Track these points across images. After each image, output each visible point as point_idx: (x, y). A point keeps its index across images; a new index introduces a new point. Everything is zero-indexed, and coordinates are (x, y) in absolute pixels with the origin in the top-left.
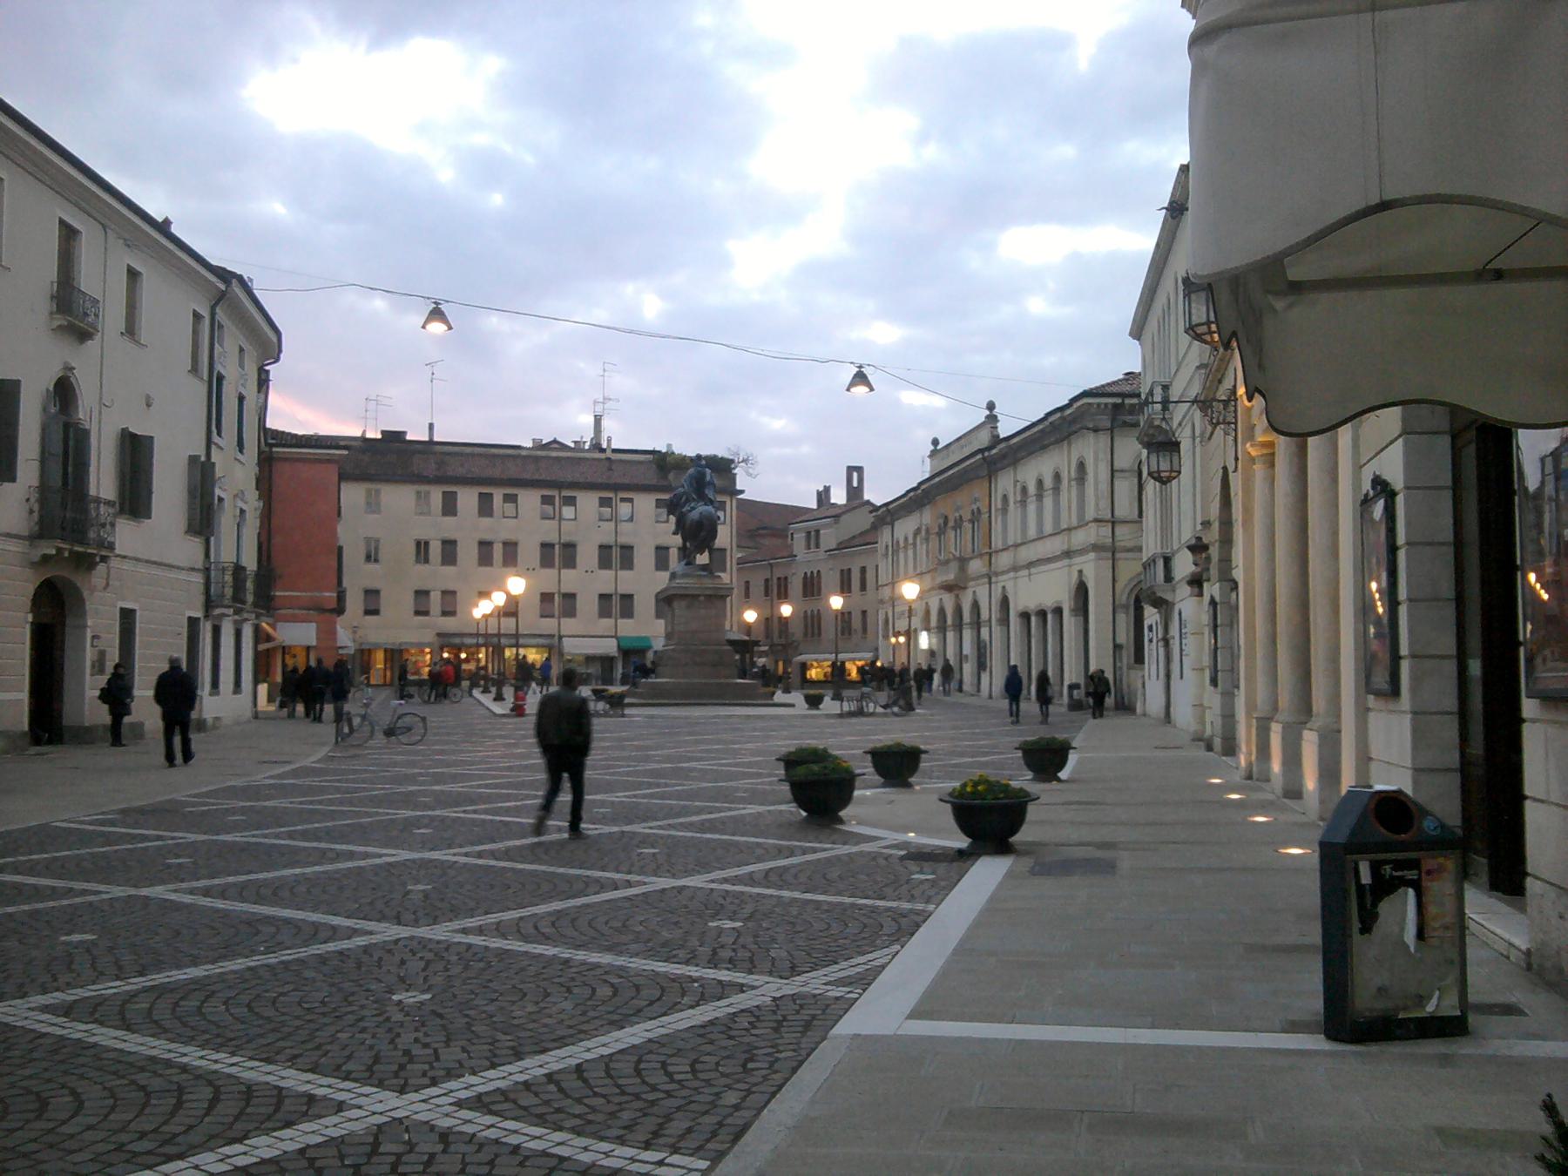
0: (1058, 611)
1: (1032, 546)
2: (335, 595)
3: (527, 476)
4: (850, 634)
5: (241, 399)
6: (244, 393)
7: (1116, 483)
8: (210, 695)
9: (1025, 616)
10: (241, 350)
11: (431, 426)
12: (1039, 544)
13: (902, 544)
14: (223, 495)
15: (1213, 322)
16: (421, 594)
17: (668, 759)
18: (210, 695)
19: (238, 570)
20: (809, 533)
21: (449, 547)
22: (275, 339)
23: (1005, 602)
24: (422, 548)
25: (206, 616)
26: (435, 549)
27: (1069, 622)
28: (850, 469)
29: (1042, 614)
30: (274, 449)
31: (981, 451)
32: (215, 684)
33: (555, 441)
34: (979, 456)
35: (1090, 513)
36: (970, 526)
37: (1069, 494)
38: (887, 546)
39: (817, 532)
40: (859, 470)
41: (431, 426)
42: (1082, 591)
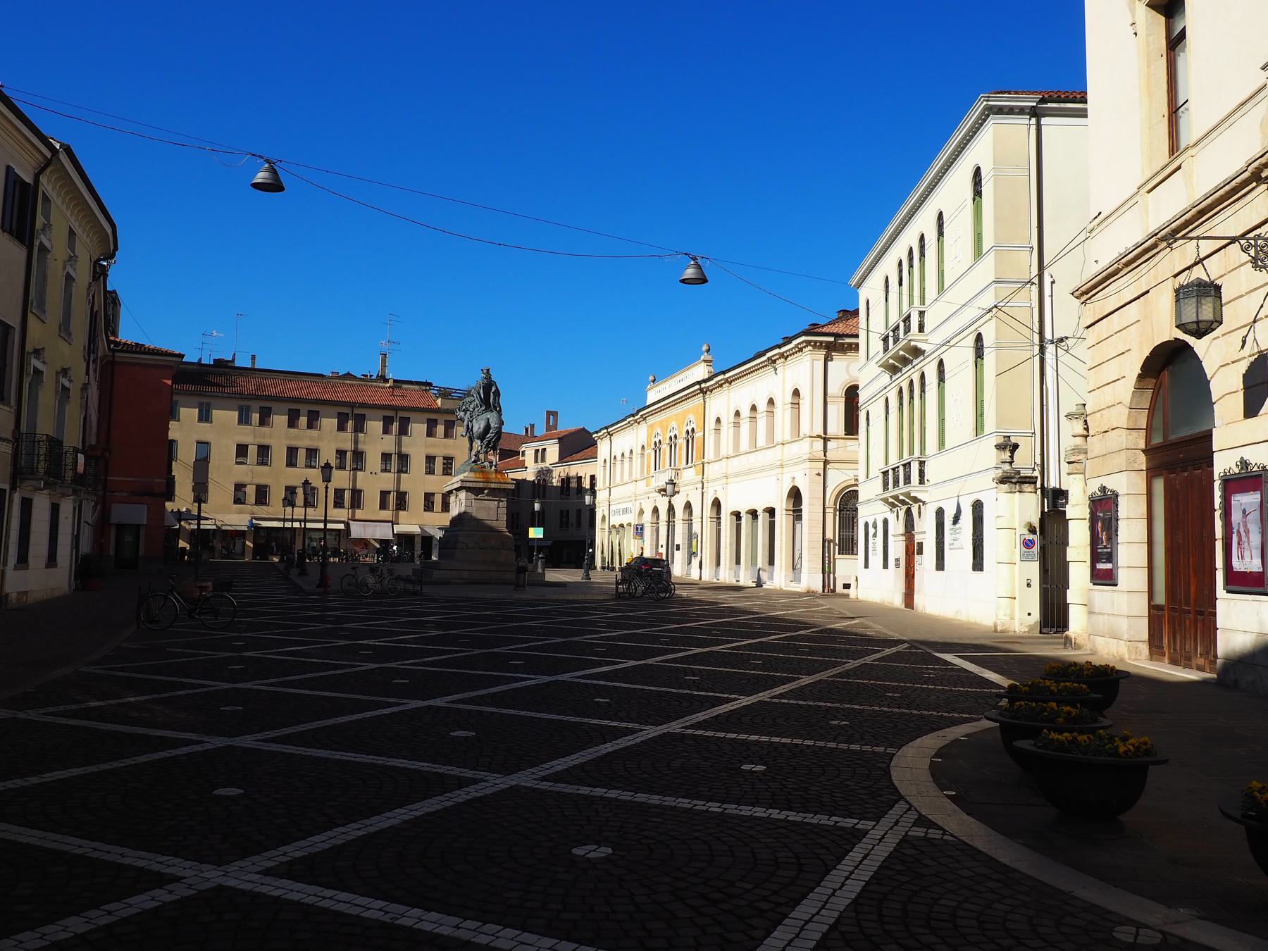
0: (771, 512)
1: (743, 458)
2: (165, 481)
3: (327, 397)
4: (567, 527)
5: (69, 279)
6: (72, 273)
7: (829, 407)
8: (16, 568)
9: (737, 515)
10: (72, 233)
11: (253, 357)
12: (735, 461)
13: (619, 457)
14: (40, 366)
15: (325, 525)
16: (239, 487)
17: (439, 625)
18: (16, 568)
19: (55, 444)
20: (538, 450)
21: (264, 451)
22: (109, 231)
23: (717, 504)
24: (242, 450)
25: (13, 488)
26: (252, 451)
27: (782, 520)
28: (549, 413)
29: (754, 514)
30: (117, 354)
31: (699, 383)
32: (23, 559)
33: (348, 374)
34: (697, 387)
35: (805, 429)
36: (669, 448)
37: (783, 412)
38: (605, 461)
39: (544, 450)
40: (555, 414)
41: (253, 357)
42: (795, 495)
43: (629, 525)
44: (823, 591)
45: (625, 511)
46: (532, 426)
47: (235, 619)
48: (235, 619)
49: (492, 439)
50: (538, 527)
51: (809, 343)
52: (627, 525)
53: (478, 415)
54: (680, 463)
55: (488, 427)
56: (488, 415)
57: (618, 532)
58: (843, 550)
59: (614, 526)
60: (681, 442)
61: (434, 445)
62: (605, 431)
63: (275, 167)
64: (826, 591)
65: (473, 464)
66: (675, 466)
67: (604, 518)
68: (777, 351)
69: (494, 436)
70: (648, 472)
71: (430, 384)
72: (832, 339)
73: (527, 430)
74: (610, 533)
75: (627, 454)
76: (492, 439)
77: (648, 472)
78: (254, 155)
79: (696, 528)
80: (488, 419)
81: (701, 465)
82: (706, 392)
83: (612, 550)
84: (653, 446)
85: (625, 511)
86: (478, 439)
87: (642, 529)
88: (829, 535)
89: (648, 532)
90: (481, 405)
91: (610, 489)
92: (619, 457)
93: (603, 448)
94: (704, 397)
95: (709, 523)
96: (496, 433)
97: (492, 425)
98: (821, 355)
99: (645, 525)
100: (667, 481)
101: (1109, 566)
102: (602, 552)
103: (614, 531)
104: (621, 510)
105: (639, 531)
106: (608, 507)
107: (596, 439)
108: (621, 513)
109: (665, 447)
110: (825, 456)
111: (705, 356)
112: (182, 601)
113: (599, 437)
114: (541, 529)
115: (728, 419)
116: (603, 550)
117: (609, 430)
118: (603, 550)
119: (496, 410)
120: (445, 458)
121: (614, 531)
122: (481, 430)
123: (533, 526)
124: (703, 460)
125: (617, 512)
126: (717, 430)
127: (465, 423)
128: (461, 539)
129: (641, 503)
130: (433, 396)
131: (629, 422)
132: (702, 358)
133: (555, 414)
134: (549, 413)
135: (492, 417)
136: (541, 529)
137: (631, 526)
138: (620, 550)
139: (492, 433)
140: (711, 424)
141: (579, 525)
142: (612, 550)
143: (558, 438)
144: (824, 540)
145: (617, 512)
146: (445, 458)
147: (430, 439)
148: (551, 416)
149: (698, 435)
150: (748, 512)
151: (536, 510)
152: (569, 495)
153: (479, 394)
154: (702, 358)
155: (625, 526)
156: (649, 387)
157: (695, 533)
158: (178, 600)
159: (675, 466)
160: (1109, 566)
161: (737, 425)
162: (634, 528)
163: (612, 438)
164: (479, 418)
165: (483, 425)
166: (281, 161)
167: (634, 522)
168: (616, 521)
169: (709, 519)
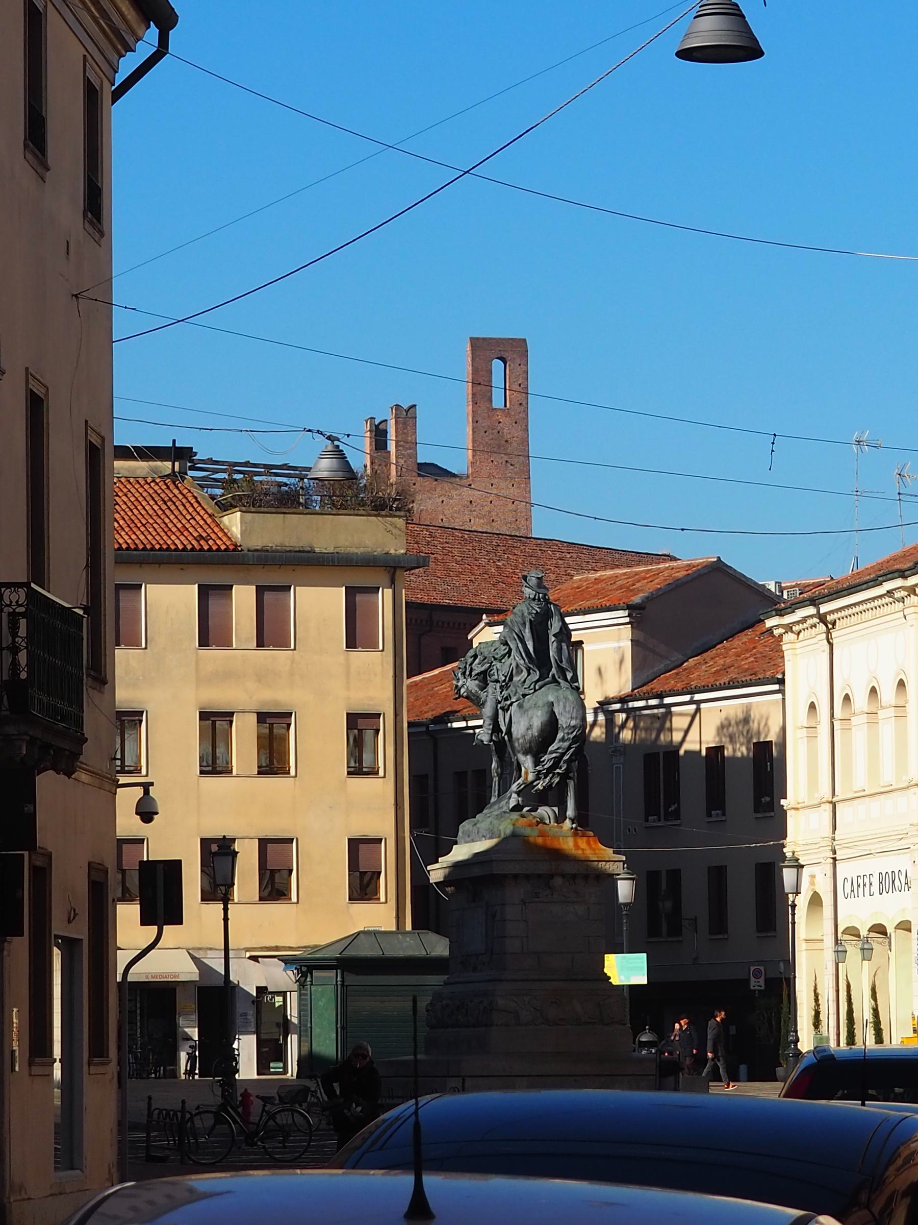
13: (860, 700)
47: (312, 1143)
48: (312, 1143)
49: (563, 754)
53: (524, 696)
55: (551, 727)
56: (549, 694)
57: (866, 953)
59: (853, 932)
61: (226, 675)
62: (811, 610)
65: (515, 815)
67: (816, 901)
69: (569, 748)
71: (182, 454)
73: (379, 435)
74: (840, 954)
75: (888, 694)
76: (563, 754)
78: (310, 431)
83: (850, 1012)
86: (525, 753)
92: (860, 700)
96: (575, 740)
97: (563, 721)
101: (757, 992)
102: (817, 1023)
103: (853, 951)
104: (875, 881)
106: (829, 869)
112: (239, 1120)
113: (789, 628)
116: (817, 1014)
117: (824, 608)
118: (817, 1014)
119: (566, 679)
120: (262, 717)
121: (853, 951)
122: (535, 732)
123: (617, 949)
125: (860, 885)
127: (488, 710)
128: (501, 1002)
130: (210, 507)
131: (890, 593)
137: (909, 930)
138: (876, 1011)
139: (563, 740)
142: (850, 1012)
145: (860, 885)
146: (262, 717)
147: (213, 654)
148: (497, 365)
151: (622, 899)
152: (677, 815)
155: (890, 930)
158: (235, 1122)
160: (757, 992)
164: (528, 702)
165: (538, 719)
166: (348, 436)
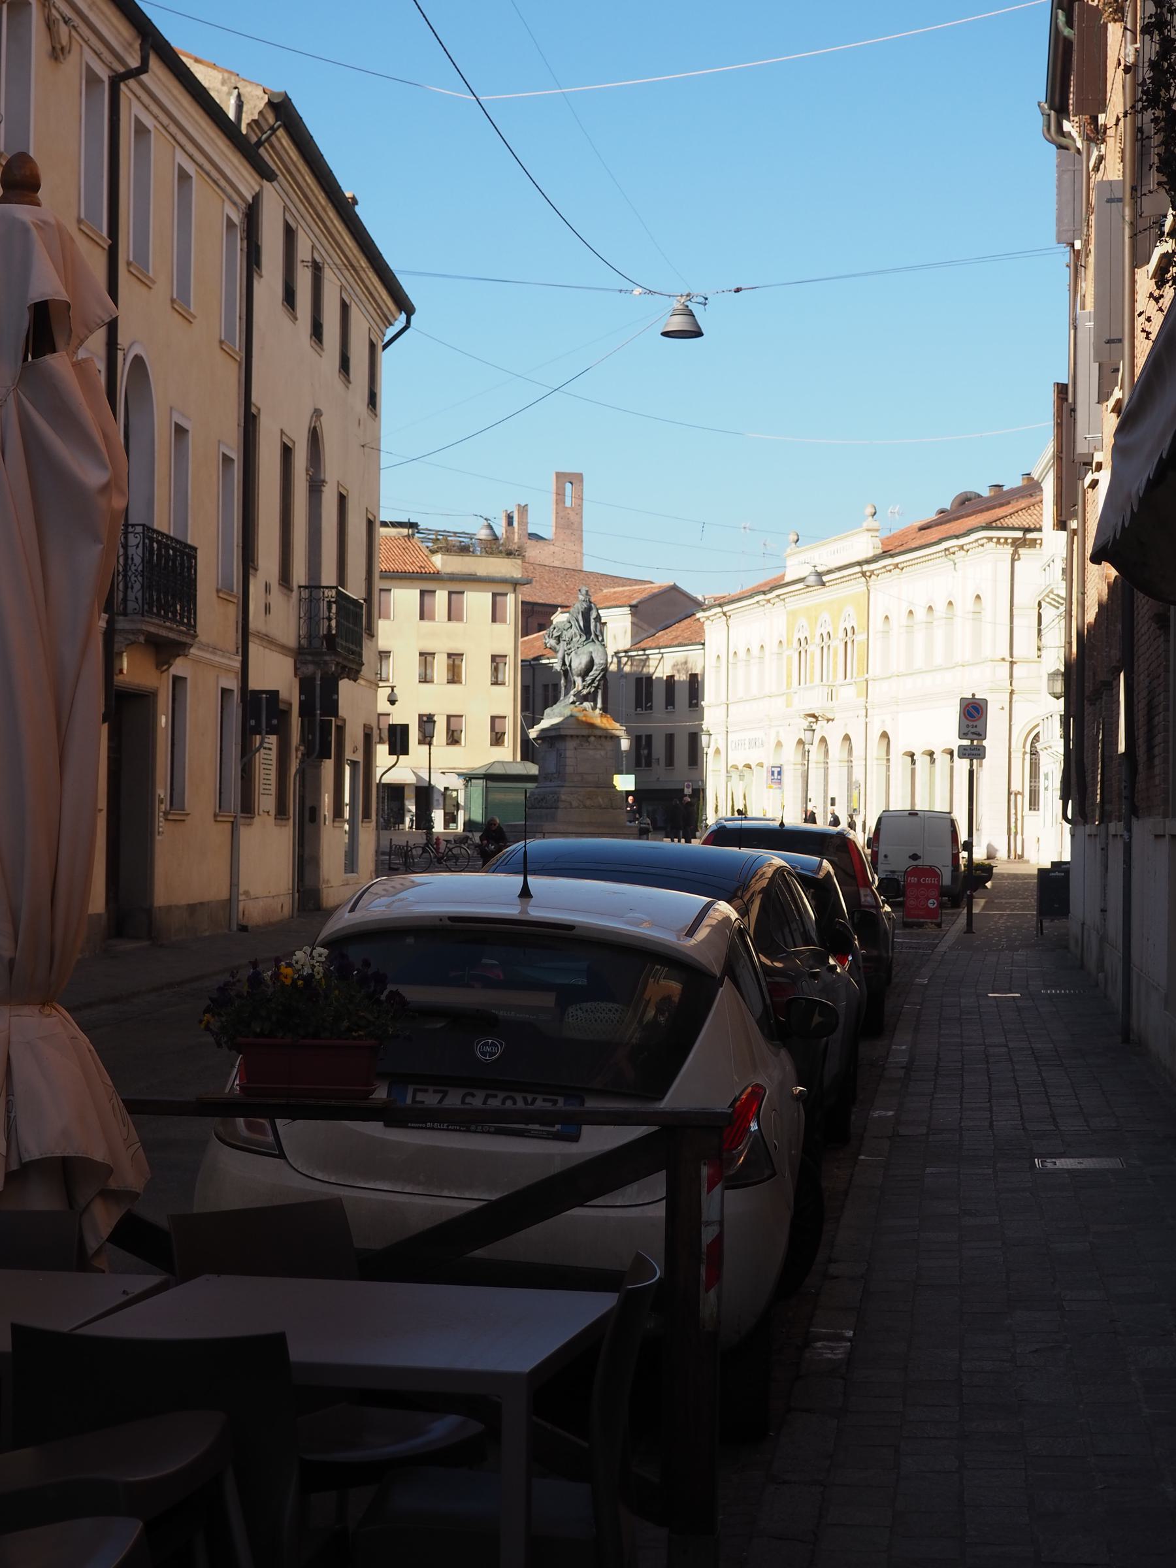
13: (742, 654)
28: (563, 478)
31: (859, 564)
43: (761, 765)
44: (1009, 857)
45: (754, 743)
46: (523, 509)
50: (627, 773)
51: (990, 539)
52: (757, 765)
54: (835, 676)
55: (591, 664)
56: (590, 647)
57: (741, 777)
58: (1035, 805)
59: (735, 767)
60: (837, 644)
62: (719, 610)
63: (492, 524)
64: (1012, 856)
66: (828, 681)
67: (717, 751)
68: (954, 542)
70: (789, 685)
72: (1019, 534)
74: (729, 777)
77: (789, 685)
79: (858, 775)
80: (591, 652)
81: (865, 682)
82: (870, 577)
84: (796, 644)
85: (754, 743)
86: (578, 676)
87: (779, 773)
88: (1016, 787)
89: (791, 778)
90: (580, 635)
91: (728, 705)
92: (742, 654)
93: (713, 626)
94: (867, 582)
95: (875, 766)
97: (596, 661)
98: (1009, 550)
99: (785, 768)
100: (806, 728)
103: (735, 775)
104: (747, 742)
105: (777, 775)
107: (702, 620)
108: (747, 746)
109: (813, 649)
110: (1011, 685)
111: (870, 523)
113: (708, 618)
114: (632, 778)
115: (899, 619)
120: (449, 655)
121: (735, 775)
123: (620, 773)
124: (866, 676)
126: (886, 632)
127: (560, 655)
129: (778, 732)
130: (427, 552)
132: (865, 525)
133: (575, 479)
134: (563, 478)
135: (593, 649)
136: (632, 778)
139: (596, 670)
140: (876, 622)
141: (670, 761)
143: (630, 606)
144: (1010, 793)
146: (449, 655)
147: (426, 624)
149: (860, 637)
150: (945, 751)
152: (651, 708)
153: (577, 621)
154: (865, 525)
155: (753, 767)
156: (788, 551)
157: (857, 782)
159: (828, 681)
161: (910, 628)
162: (768, 772)
163: (730, 621)
167: (769, 762)
168: (738, 758)
169: (875, 762)
